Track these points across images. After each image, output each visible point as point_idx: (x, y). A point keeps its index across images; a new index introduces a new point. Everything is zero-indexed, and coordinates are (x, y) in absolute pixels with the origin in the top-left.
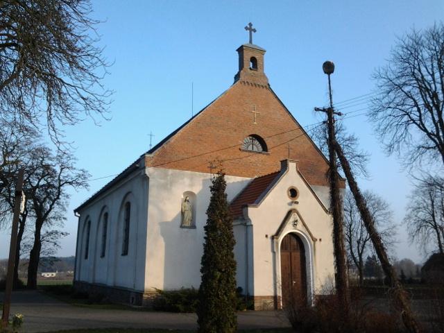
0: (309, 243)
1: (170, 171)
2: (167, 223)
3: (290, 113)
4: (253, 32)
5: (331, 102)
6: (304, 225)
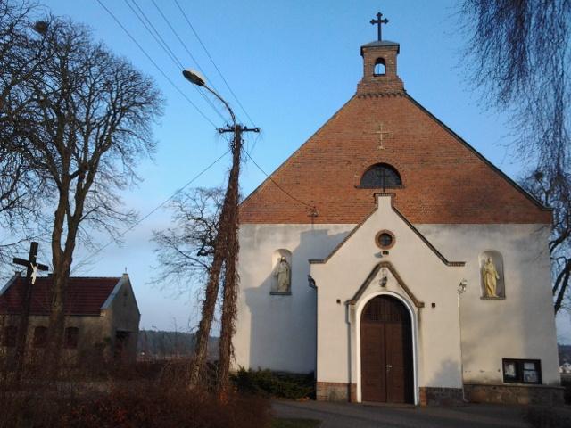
0: (412, 310)
1: (258, 227)
2: (253, 290)
5: (224, 119)
6: (401, 283)
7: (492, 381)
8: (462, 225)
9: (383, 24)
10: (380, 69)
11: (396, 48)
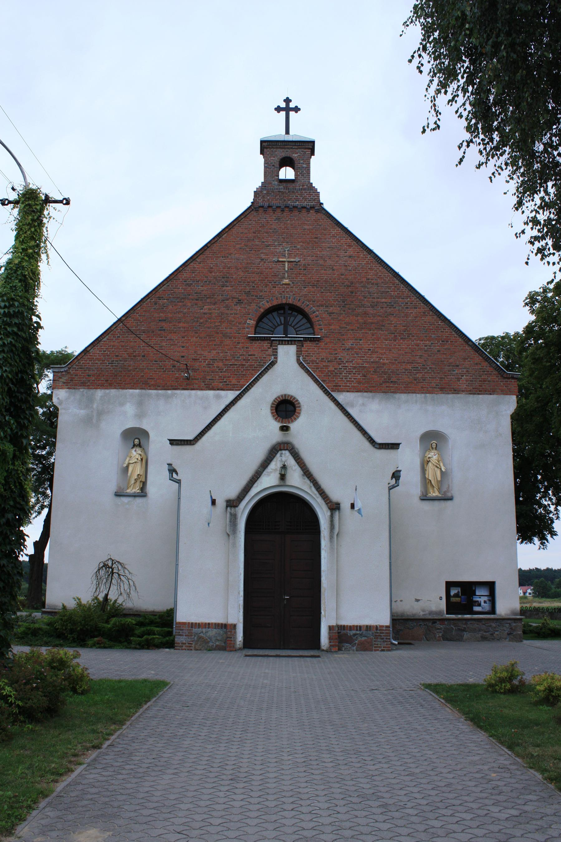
1: (99, 393)
6: (307, 473)
7: (431, 613)
8: (397, 396)
9: (292, 114)
10: (287, 173)
11: (309, 147)
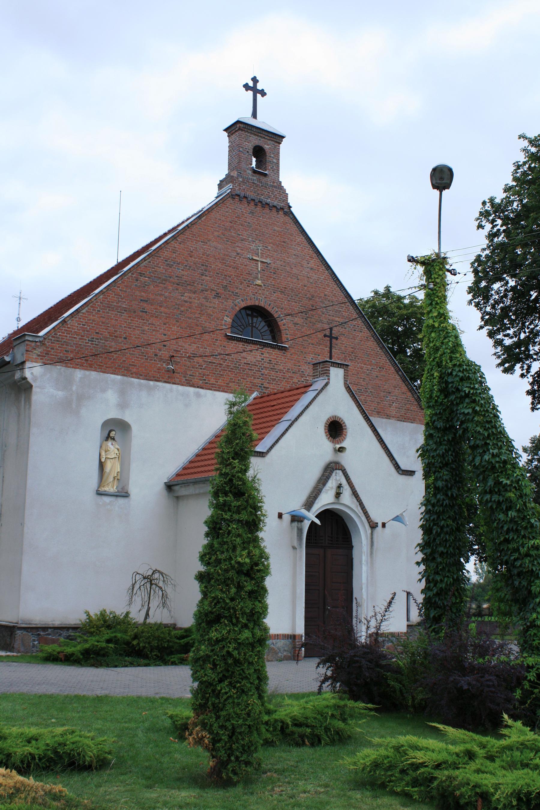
1: (79, 374)
3: (328, 267)
4: (259, 96)
6: (355, 494)
